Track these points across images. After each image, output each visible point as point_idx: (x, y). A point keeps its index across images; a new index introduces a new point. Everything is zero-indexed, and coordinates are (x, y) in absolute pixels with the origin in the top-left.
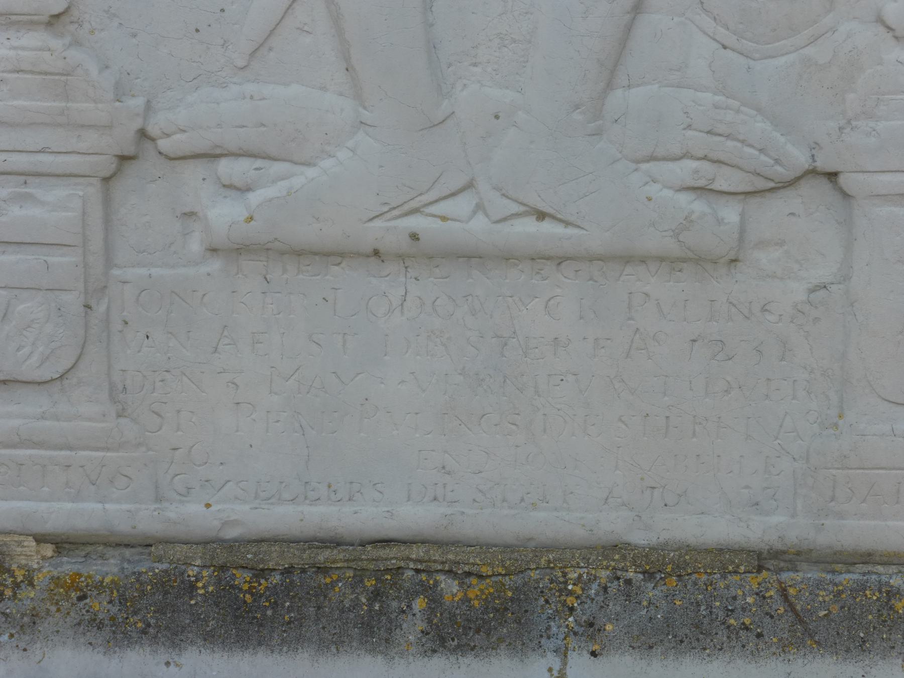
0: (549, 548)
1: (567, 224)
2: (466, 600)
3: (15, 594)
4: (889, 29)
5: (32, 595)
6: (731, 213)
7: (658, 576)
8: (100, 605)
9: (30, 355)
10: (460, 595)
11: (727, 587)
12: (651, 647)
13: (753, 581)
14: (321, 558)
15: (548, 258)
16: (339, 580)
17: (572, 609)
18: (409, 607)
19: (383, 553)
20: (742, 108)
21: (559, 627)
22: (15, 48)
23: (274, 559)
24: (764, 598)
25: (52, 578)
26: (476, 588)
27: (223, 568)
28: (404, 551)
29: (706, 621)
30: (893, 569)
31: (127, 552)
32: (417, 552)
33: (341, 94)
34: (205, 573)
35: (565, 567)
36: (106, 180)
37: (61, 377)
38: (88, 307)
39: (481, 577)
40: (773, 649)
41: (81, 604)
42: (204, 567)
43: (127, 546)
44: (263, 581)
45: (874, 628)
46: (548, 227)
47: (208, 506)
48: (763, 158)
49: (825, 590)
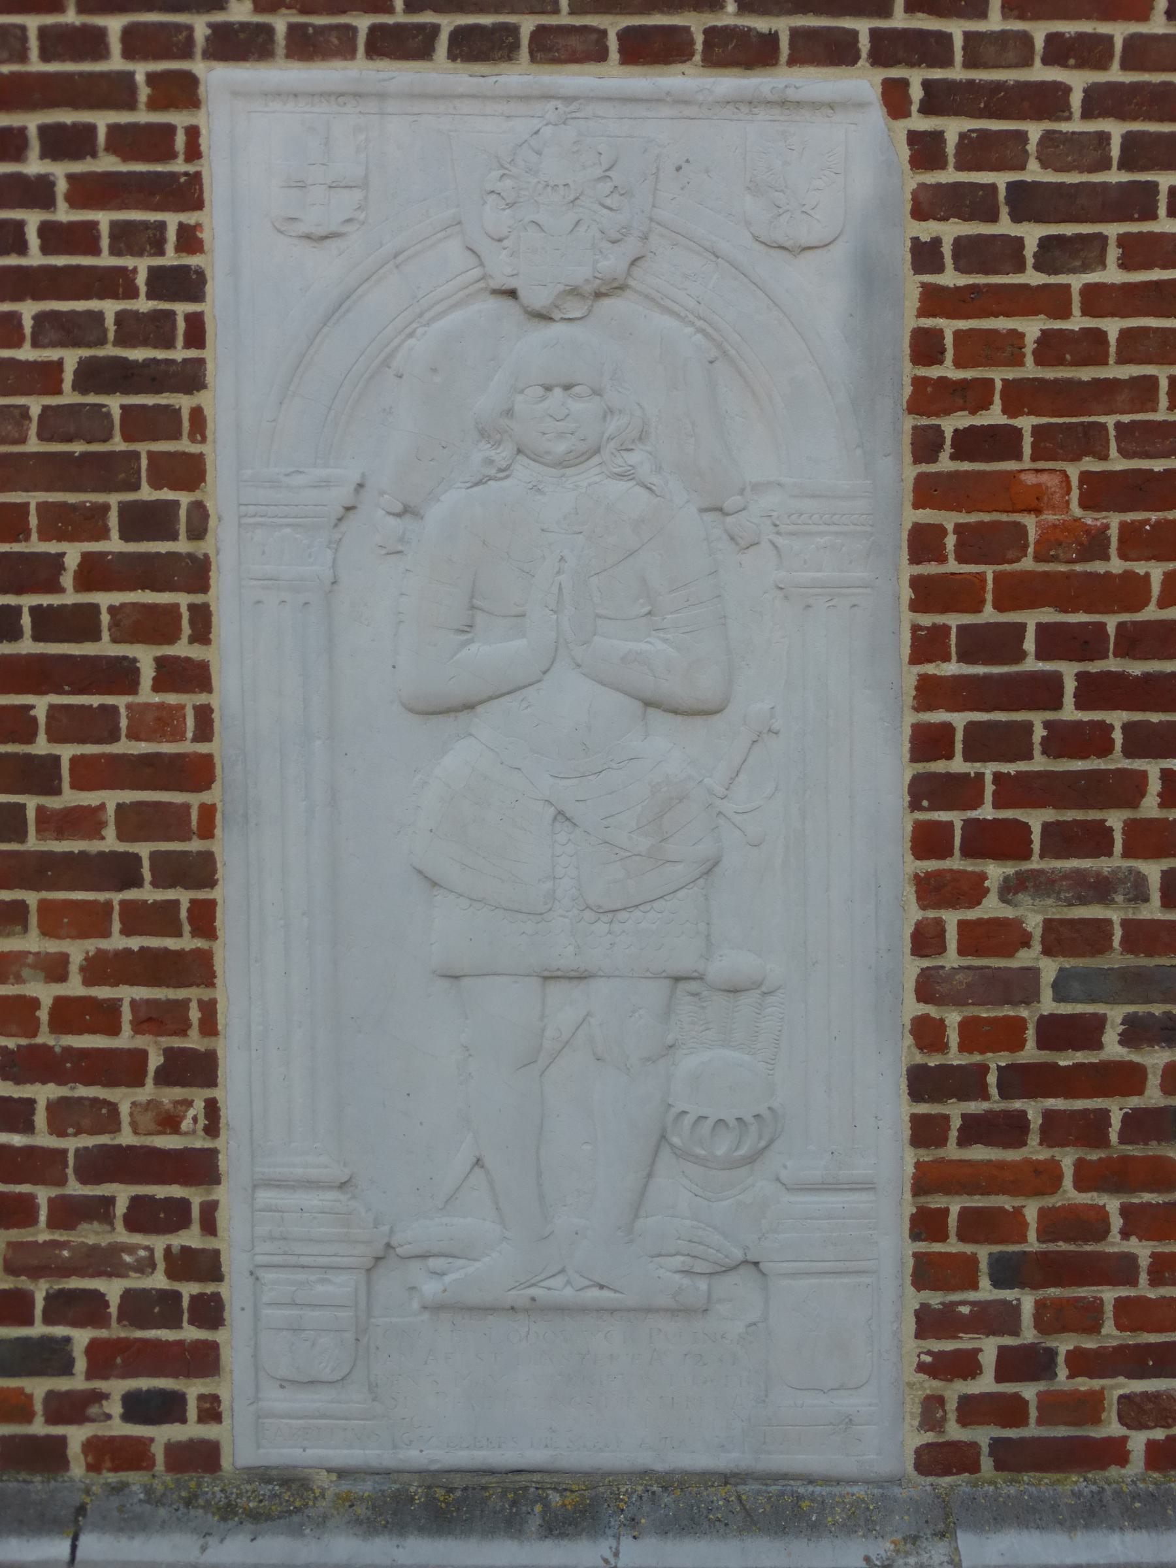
0: (610, 1474)
1: (616, 1291)
2: (564, 1505)
3: (314, 1504)
4: (783, 1184)
5: (324, 1504)
6: (703, 1284)
7: (670, 1489)
8: (361, 1510)
9: (488, 612)
10: (560, 1503)
11: (708, 1495)
12: (666, 1533)
13: (722, 1491)
14: (483, 1481)
15: (606, 1310)
16: (493, 1494)
17: (622, 1510)
18: (532, 1510)
19: (518, 1478)
20: (707, 1228)
21: (616, 1521)
22: (321, 1200)
23: (458, 1482)
24: (729, 1501)
25: (336, 1494)
26: (570, 1498)
27: (429, 1487)
28: (529, 1476)
29: (697, 1516)
30: (799, 1483)
31: (377, 1478)
32: (537, 1477)
33: (493, 1222)
34: (420, 1490)
35: (619, 1484)
36: (368, 1270)
37: (342, 1379)
38: (357, 1340)
39: (572, 1491)
40: (734, 1533)
41: (351, 1510)
42: (419, 1486)
43: (378, 1474)
44: (451, 1495)
45: (790, 1519)
46: (606, 1293)
47: (421, 1451)
48: (719, 1255)
49: (762, 1496)
